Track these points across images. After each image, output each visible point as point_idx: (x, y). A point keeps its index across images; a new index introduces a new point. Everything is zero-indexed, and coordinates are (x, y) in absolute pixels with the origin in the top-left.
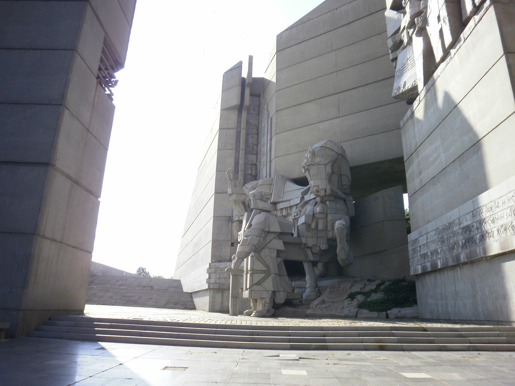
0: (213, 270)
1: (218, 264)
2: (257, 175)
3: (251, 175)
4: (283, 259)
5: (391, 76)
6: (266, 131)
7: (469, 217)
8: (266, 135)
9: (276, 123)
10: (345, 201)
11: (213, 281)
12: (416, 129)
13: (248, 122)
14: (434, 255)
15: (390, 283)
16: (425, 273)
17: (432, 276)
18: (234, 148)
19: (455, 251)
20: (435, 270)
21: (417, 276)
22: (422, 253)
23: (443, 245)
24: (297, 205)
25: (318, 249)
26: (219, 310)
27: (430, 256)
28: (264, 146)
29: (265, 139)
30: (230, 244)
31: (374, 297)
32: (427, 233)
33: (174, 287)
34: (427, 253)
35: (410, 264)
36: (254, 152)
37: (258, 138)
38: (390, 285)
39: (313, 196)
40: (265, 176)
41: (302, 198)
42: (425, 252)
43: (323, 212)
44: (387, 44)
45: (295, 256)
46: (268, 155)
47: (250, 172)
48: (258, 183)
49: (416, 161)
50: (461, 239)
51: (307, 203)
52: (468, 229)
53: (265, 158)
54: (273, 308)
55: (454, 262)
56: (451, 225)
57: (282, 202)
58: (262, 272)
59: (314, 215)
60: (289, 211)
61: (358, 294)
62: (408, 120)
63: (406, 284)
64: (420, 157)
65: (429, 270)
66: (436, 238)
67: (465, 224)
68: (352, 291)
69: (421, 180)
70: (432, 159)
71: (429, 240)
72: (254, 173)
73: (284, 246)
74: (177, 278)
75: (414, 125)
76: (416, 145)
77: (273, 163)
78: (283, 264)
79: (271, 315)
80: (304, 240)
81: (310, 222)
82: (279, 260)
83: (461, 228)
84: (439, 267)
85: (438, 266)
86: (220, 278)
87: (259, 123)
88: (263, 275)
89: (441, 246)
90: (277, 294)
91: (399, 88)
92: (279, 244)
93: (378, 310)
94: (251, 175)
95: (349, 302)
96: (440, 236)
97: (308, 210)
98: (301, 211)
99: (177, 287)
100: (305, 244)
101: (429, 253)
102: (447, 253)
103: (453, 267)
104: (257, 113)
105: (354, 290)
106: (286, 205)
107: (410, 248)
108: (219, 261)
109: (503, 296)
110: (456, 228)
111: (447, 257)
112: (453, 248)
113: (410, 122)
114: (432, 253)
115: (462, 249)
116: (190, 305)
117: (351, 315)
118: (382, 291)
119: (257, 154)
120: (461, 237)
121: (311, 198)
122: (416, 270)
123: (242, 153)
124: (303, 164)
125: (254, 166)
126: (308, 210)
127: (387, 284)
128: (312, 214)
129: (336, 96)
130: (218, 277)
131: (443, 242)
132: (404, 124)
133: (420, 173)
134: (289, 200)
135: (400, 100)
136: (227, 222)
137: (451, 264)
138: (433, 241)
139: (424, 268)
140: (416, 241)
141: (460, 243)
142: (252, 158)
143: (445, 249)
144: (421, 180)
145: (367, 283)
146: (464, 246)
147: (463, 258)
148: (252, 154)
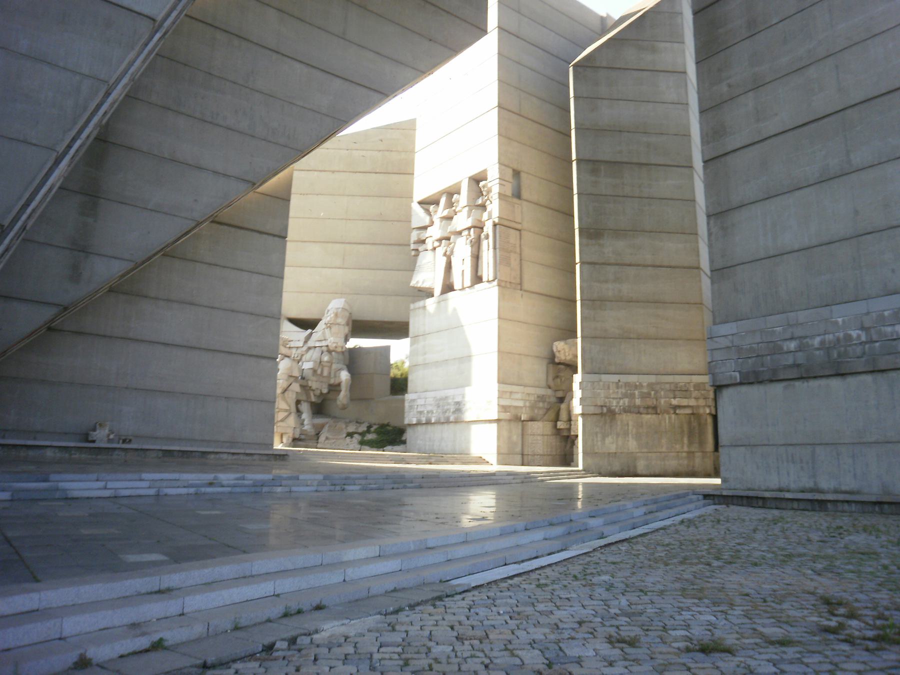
5: (411, 267)
16: (419, 423)
17: (424, 427)
19: (447, 414)
20: (428, 423)
21: (410, 425)
24: (297, 348)
41: (306, 342)
43: (330, 362)
52: (458, 403)
56: (446, 398)
58: (286, 410)
67: (457, 400)
88: (286, 414)
91: (418, 282)
92: (296, 387)
105: (351, 429)
109: (468, 441)
129: (343, 245)
131: (439, 407)
133: (425, 354)
138: (431, 405)
140: (414, 400)
146: (454, 412)
147: (452, 419)
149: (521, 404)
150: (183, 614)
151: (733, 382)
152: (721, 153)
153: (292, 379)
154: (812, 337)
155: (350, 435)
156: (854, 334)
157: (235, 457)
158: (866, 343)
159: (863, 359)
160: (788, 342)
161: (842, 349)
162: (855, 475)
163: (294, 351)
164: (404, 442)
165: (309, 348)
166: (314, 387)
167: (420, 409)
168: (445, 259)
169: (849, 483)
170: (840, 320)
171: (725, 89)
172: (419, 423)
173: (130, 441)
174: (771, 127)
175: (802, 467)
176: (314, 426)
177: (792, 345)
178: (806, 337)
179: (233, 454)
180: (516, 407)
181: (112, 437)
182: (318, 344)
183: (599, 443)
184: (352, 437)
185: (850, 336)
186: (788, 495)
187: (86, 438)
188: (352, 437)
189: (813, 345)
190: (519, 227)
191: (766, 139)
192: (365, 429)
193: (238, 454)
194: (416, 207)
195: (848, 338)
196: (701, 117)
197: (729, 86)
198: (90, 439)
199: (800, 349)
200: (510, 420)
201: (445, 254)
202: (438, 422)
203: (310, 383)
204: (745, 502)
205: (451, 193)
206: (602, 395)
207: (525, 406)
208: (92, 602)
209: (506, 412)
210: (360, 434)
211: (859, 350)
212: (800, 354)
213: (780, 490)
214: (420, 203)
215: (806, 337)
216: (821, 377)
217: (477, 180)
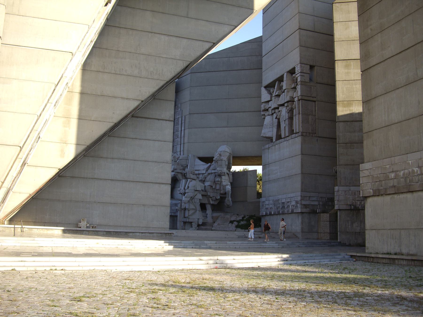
6: (180, 123)
7: (284, 199)
8: (180, 125)
16: (266, 215)
17: (269, 217)
20: (270, 214)
21: (263, 216)
22: (266, 207)
25: (215, 198)
31: (242, 223)
41: (207, 170)
44: (261, 107)
45: (205, 201)
50: (281, 206)
56: (278, 200)
67: (283, 201)
92: (199, 196)
103: (277, 215)
105: (233, 218)
107: (261, 204)
110: (280, 202)
120: (281, 205)
122: (263, 213)
127: (247, 217)
133: (269, 175)
134: (198, 170)
137: (277, 213)
138: (271, 204)
139: (266, 213)
140: (264, 202)
146: (282, 209)
148: (221, 182)
149: (316, 203)
151: (370, 195)
152: (368, 67)
153: (196, 192)
154: (400, 171)
155: (232, 222)
156: (415, 169)
157: (143, 234)
158: (420, 175)
159: (418, 184)
160: (391, 174)
161: (411, 178)
162: (415, 246)
163: (201, 176)
165: (209, 174)
166: (211, 196)
167: (267, 207)
168: (277, 120)
169: (413, 251)
170: (410, 162)
171: (369, 31)
172: (266, 215)
173: (95, 227)
174: (388, 53)
175: (396, 241)
176: (212, 217)
177: (392, 175)
178: (397, 171)
179: (142, 233)
180: (313, 205)
181: (88, 225)
182: (213, 171)
183: (350, 226)
184: (232, 223)
185: (414, 170)
186: (380, 256)
187: (77, 226)
188: (232, 223)
189: (400, 176)
190: (314, 99)
191: (386, 60)
192: (241, 218)
193: (153, 233)
194: (263, 89)
195: (413, 171)
196: (360, 46)
197: (371, 30)
198: (79, 226)
199: (395, 178)
200: (309, 213)
201: (276, 118)
202: (275, 214)
203: (209, 194)
205: (280, 79)
206: (351, 199)
207: (319, 205)
209: (306, 208)
210: (237, 221)
211: (417, 178)
212: (395, 180)
213: (388, 254)
214: (266, 87)
215: (397, 171)
216: (404, 192)
217: (292, 72)
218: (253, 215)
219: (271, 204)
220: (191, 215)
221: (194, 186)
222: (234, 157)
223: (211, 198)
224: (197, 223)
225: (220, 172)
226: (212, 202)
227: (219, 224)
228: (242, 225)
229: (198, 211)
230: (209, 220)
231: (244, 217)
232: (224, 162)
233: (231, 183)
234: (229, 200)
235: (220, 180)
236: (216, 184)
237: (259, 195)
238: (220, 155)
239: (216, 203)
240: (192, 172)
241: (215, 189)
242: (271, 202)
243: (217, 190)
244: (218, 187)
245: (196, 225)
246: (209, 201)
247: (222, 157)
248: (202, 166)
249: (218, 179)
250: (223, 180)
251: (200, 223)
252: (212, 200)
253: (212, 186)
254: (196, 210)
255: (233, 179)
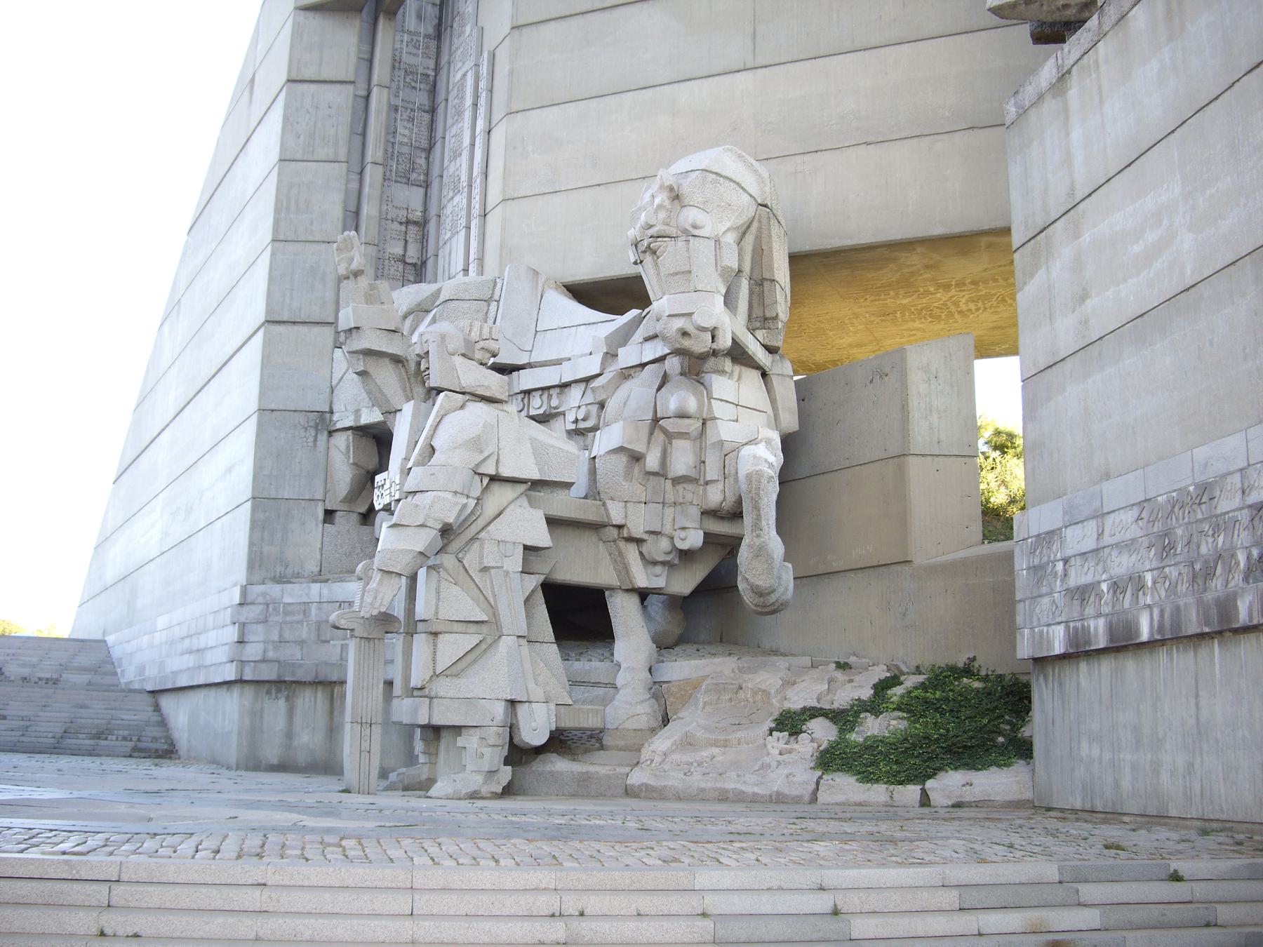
0: (254, 612)
1: (275, 590)
2: (424, 263)
3: (402, 259)
4: (543, 577)
6: (469, 101)
8: (468, 115)
9: (511, 72)
10: (764, 375)
11: (253, 651)
12: (1076, 135)
13: (396, 64)
14: (1124, 592)
15: (921, 678)
16: (1079, 653)
17: (1106, 666)
18: (342, 153)
19: (1217, 584)
20: (1123, 644)
22: (1073, 581)
23: (1167, 562)
24: (587, 380)
25: (664, 544)
26: (275, 761)
27: (1107, 597)
28: (456, 155)
29: (460, 131)
30: (321, 515)
31: (873, 727)
32: (1100, 516)
33: (84, 670)
34: (1094, 586)
35: (1019, 619)
36: (414, 176)
37: (432, 127)
38: (923, 686)
39: (653, 351)
40: (460, 266)
41: (611, 355)
42: (1087, 579)
45: (583, 566)
46: (476, 192)
47: (398, 250)
48: (439, 290)
49: (1064, 253)
51: (626, 374)
53: (461, 200)
54: (507, 762)
55: (1207, 624)
56: (1206, 491)
57: (529, 365)
59: (656, 420)
60: (554, 403)
61: (813, 716)
62: (1041, 97)
63: (977, 685)
64: (1086, 238)
65: (1102, 644)
66: (1140, 533)
68: (787, 705)
69: (1085, 322)
70: (1137, 248)
71: (1107, 540)
72: (413, 255)
73: (551, 532)
74: (91, 631)
75: (1067, 118)
76: (1071, 193)
77: (494, 220)
78: (540, 599)
79: (500, 790)
80: (616, 513)
81: (639, 447)
82: (533, 582)
83: (1250, 506)
84: (1145, 637)
85: (1137, 633)
86: (282, 641)
87: (437, 69)
89: (1155, 564)
90: (522, 711)
93: (898, 779)
94: (402, 259)
95: (781, 745)
96: (1158, 527)
97: (632, 403)
98: (602, 405)
99: (95, 670)
100: (620, 527)
101: (1104, 587)
102: (1182, 588)
104: (431, 31)
105: (798, 699)
106: (549, 377)
108: (280, 580)
110: (1227, 503)
111: (1181, 602)
112: (1209, 574)
113: (1050, 105)
114: (1116, 587)
115: (1246, 579)
116: (155, 739)
117: (795, 791)
118: (898, 709)
119: (427, 185)
120: (1243, 537)
121: (645, 360)
122: (1042, 639)
123: (373, 175)
124: (632, 233)
125: (413, 229)
126: (632, 403)
127: (911, 681)
128: (650, 416)
130: (276, 638)
132: (1023, 113)
133: (1083, 297)
134: (558, 362)
135: (1009, 22)
136: (313, 432)
137: (1192, 626)
138: (1128, 546)
140: (1048, 538)
141: (1241, 557)
142: (412, 198)
143: (1175, 574)
144: (1085, 322)
145: (840, 675)
147: (1244, 611)
148: (408, 182)
150: (56, 682)
155: (790, 723)
164: (1024, 750)
165: (626, 374)
167: (1078, 578)
172: (1079, 653)
176: (657, 690)
184: (795, 732)
192: (866, 693)
202: (1172, 638)
204: (731, 796)
208: (40, 753)
210: (835, 716)
218: (961, 661)
219: (1128, 546)
220: (455, 670)
221: (476, 443)
222: (804, 263)
223: (639, 541)
224: (496, 736)
225: (679, 323)
226: (642, 581)
227: (688, 743)
228: (871, 746)
229: (506, 643)
230: (628, 706)
231: (894, 681)
232: (703, 250)
233: (789, 444)
234: (765, 559)
235: (692, 404)
236: (670, 436)
237: (996, 522)
238: (676, 197)
239: (685, 583)
240: (470, 344)
241: (661, 474)
242: (1124, 525)
243: (677, 481)
244: (682, 461)
245: (493, 756)
246: (624, 569)
247: (690, 215)
248: (581, 336)
249: (679, 398)
250: (718, 409)
251: (534, 732)
252: (649, 562)
253: (637, 458)
254: (488, 628)
255: (803, 415)
